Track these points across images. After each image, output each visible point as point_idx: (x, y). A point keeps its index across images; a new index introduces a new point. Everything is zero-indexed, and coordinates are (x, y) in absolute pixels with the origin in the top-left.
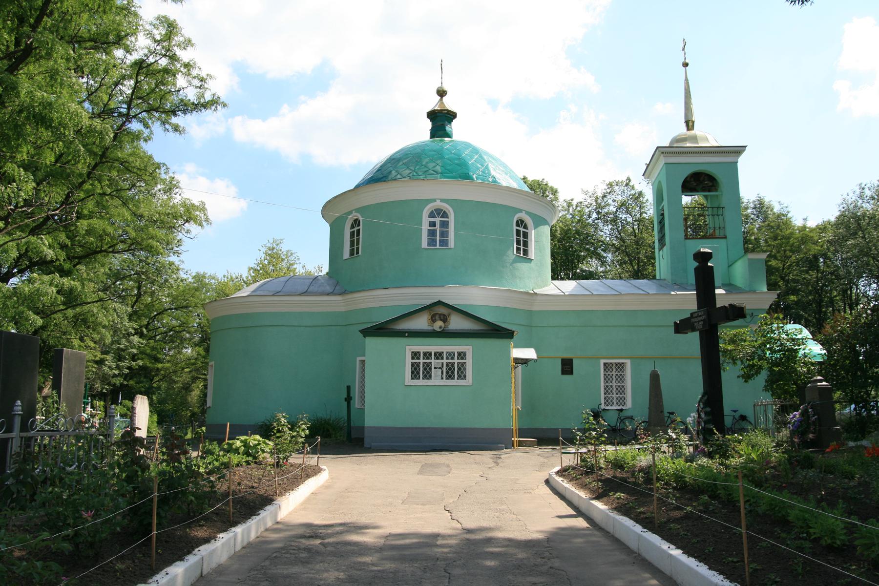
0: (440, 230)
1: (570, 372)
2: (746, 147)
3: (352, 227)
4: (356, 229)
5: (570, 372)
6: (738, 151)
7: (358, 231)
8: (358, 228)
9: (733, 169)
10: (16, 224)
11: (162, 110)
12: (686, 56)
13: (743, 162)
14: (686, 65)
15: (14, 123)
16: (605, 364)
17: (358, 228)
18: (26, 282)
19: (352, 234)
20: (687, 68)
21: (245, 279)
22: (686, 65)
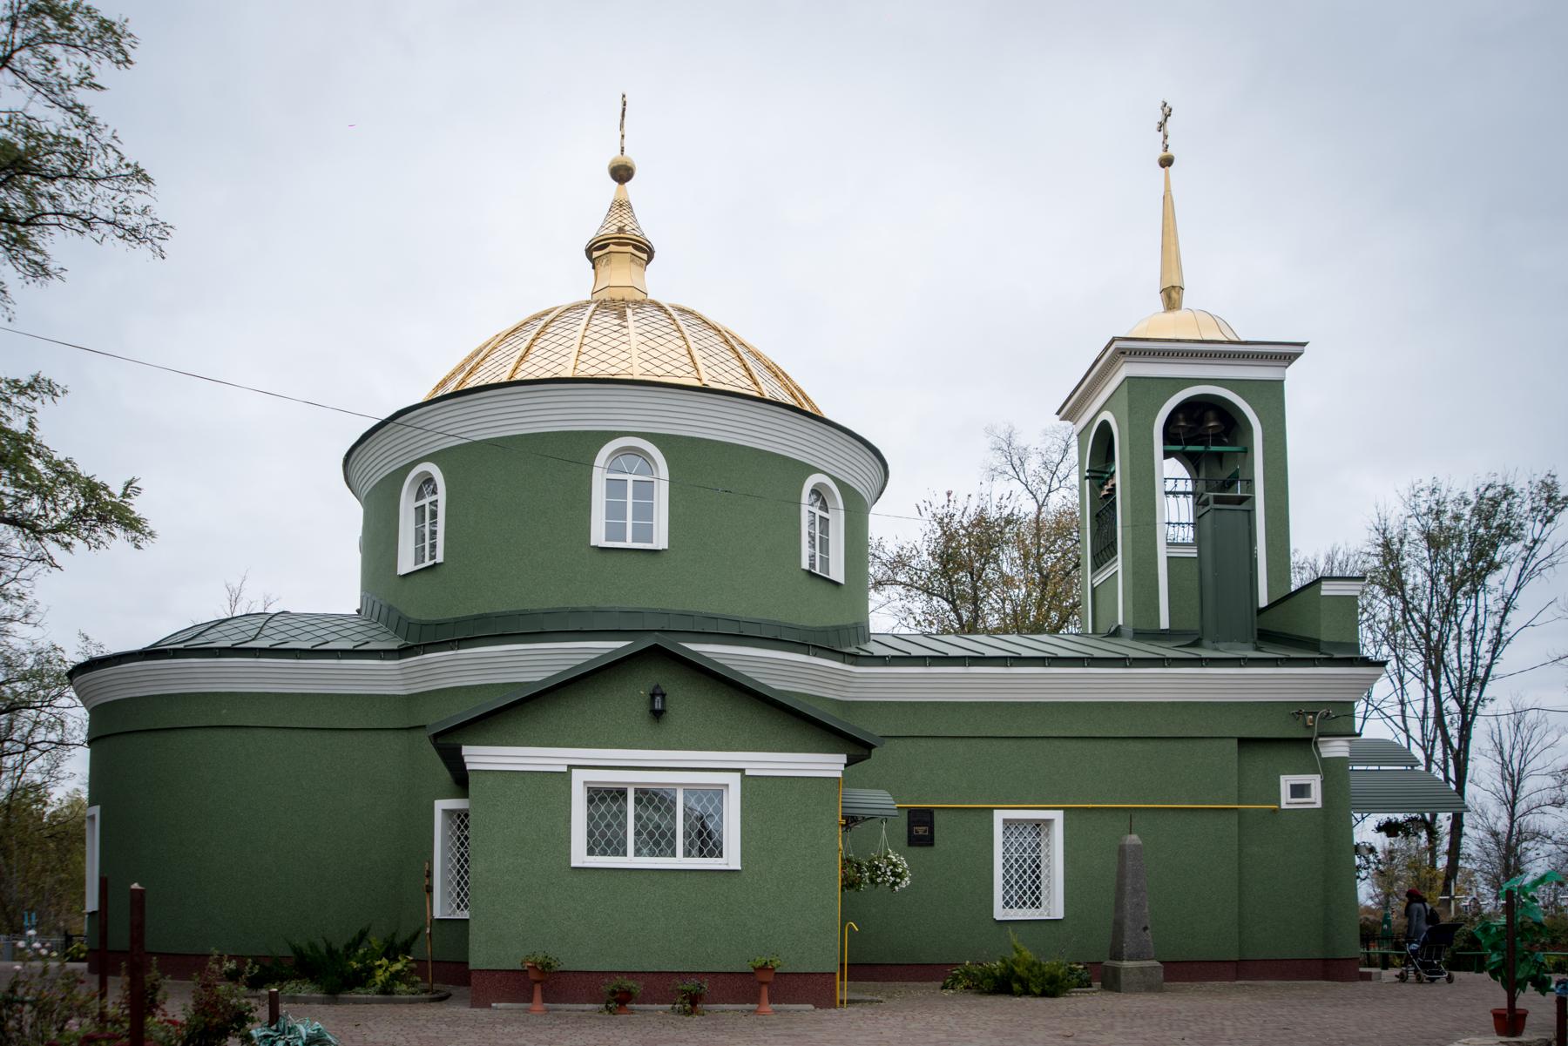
0: (625, 497)
1: (928, 841)
2: (1304, 344)
3: (420, 496)
4: (426, 501)
5: (928, 841)
6: (1286, 355)
7: (434, 503)
8: (433, 498)
9: (1271, 396)
10: (72, 163)
11: (1055, 468)
12: (1169, 141)
13: (1294, 377)
14: (1166, 162)
15: (619, 224)
16: (1005, 821)
17: (433, 498)
18: (57, 162)
19: (420, 511)
20: (1171, 169)
21: (96, 528)
22: (622, 173)
